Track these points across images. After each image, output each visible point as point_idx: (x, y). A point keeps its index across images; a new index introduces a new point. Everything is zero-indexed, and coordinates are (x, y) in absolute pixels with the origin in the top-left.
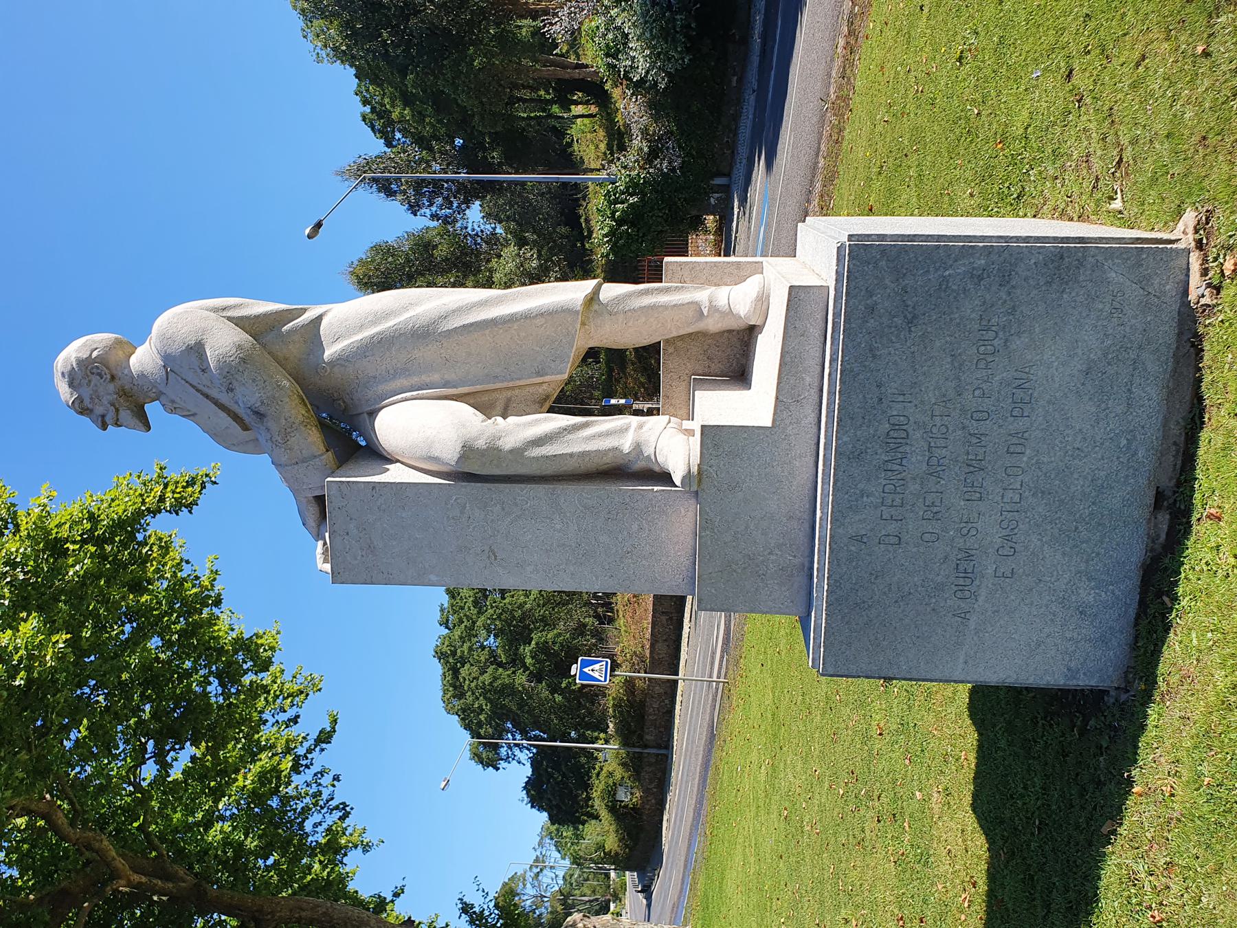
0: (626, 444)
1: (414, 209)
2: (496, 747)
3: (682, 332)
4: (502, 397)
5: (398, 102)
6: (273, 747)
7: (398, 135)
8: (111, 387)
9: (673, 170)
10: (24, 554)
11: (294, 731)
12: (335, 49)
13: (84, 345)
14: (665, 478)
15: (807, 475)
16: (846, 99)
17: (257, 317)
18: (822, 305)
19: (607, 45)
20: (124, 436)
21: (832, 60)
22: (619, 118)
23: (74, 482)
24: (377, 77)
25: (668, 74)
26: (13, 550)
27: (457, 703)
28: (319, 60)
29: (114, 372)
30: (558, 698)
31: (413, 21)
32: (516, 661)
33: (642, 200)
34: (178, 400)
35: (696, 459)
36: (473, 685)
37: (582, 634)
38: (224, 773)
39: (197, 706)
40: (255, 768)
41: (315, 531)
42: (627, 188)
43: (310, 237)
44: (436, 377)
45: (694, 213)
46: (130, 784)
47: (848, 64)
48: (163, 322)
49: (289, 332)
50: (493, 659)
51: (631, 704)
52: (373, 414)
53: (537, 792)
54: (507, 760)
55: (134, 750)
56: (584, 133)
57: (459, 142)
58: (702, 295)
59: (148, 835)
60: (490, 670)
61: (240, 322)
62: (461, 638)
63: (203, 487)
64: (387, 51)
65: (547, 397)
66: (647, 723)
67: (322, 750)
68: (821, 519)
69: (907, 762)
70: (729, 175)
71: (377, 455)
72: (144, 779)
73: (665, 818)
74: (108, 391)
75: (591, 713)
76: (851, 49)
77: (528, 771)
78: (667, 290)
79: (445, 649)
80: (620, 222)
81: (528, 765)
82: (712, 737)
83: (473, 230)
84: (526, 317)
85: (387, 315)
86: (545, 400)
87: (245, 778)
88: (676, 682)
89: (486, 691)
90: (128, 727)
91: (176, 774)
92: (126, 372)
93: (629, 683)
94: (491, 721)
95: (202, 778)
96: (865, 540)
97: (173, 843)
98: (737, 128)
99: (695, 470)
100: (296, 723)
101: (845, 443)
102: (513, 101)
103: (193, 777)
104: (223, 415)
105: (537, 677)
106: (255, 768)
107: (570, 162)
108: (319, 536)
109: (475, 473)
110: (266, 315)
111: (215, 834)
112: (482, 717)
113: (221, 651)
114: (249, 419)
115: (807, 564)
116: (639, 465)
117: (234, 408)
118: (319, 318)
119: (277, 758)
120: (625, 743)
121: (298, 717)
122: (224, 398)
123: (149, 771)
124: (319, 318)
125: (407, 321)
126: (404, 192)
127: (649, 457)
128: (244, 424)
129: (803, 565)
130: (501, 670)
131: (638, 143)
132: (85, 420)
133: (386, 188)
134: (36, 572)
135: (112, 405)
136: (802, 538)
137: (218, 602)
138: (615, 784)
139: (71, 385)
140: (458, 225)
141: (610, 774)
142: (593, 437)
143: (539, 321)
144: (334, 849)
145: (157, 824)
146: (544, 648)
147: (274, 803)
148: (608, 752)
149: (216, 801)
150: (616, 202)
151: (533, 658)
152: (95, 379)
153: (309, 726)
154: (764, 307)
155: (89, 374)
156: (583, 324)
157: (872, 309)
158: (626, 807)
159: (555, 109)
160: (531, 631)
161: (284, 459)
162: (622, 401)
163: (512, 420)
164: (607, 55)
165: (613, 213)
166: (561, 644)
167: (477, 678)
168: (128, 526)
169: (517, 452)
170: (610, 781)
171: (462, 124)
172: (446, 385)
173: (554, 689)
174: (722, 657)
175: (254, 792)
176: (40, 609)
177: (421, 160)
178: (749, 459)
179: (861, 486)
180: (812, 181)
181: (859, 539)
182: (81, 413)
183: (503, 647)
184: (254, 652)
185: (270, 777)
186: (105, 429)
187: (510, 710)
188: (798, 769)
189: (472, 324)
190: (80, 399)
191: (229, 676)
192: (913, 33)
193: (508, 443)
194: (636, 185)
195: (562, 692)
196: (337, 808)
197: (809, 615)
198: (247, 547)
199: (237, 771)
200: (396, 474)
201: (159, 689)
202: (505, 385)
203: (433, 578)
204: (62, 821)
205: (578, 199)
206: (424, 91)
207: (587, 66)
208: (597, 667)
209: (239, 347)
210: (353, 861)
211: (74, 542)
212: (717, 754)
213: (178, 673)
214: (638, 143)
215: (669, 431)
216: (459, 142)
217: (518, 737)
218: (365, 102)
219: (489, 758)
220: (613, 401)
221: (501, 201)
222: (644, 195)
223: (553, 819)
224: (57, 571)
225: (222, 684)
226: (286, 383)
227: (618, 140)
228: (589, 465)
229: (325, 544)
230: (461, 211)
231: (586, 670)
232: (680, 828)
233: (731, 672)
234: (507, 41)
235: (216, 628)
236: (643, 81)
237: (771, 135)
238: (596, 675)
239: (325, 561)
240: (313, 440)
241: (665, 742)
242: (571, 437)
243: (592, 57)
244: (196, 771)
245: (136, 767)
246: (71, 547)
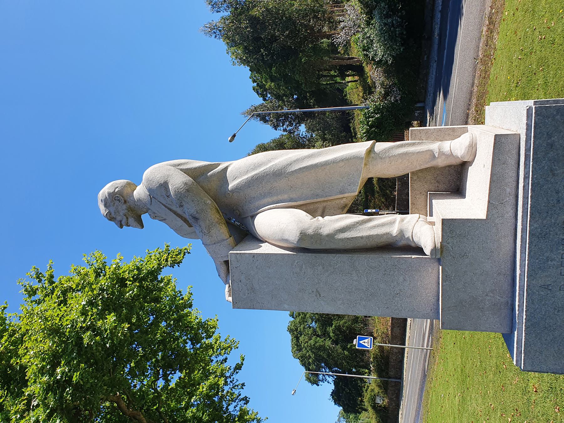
0: (394, 231)
1: (276, 127)
2: (317, 375)
3: (423, 167)
4: (321, 206)
5: (269, 80)
6: (215, 372)
7: (269, 95)
8: (124, 207)
9: (397, 101)
10: (107, 286)
11: (225, 365)
12: (241, 59)
13: (112, 185)
14: (419, 250)
15: (510, 246)
16: (488, 56)
17: (195, 168)
18: (516, 145)
19: (364, 46)
20: (131, 231)
21: (480, 39)
22: (369, 80)
23: (131, 252)
24: (259, 70)
25: (393, 57)
26: (103, 284)
27: (300, 354)
28: (234, 64)
29: (126, 199)
30: (346, 353)
31: (275, 45)
32: (325, 334)
33: (381, 116)
34: (156, 212)
35: (439, 239)
36: (306, 345)
37: (357, 322)
38: (193, 385)
39: (181, 354)
40: (208, 383)
41: (225, 279)
42: (374, 111)
43: (230, 141)
44: (286, 197)
45: (407, 120)
46: (153, 389)
47: (490, 37)
48: (147, 173)
49: (211, 176)
50: (315, 333)
52: (253, 217)
53: (337, 397)
54: (322, 381)
55: (154, 373)
56: (352, 88)
57: (295, 97)
58: (435, 146)
59: (160, 413)
60: (314, 338)
61: (187, 172)
62: (300, 322)
63: (184, 255)
64: (263, 58)
65: (346, 205)
66: (390, 367)
67: (237, 373)
68: (520, 275)
69: (557, 410)
70: (424, 102)
71: (258, 240)
72: (159, 387)
73: (400, 413)
74: (123, 208)
75: (363, 361)
76: (490, 31)
77: (332, 387)
78: (414, 144)
79: (292, 327)
80: (371, 127)
81: (333, 384)
82: (424, 376)
83: (302, 135)
84: (334, 162)
85: (260, 165)
86: (344, 207)
87: (203, 388)
88: (404, 349)
89: (312, 348)
90: (152, 363)
91: (172, 385)
92: (131, 198)
93: (381, 348)
94: (315, 362)
95: (184, 387)
96: (550, 288)
97: (171, 417)
98: (427, 79)
99: (438, 245)
100: (226, 362)
101: (536, 228)
102: (320, 77)
103: (180, 387)
104: (179, 219)
105: (336, 342)
106: (208, 383)
107: (345, 102)
108: (226, 282)
109: (309, 247)
110: (199, 168)
111: (189, 414)
112: (310, 361)
113: (192, 328)
114: (191, 221)
115: (510, 302)
116: (402, 243)
117: (184, 215)
118: (226, 168)
119: (217, 378)
120: (380, 376)
121: (226, 359)
122: (179, 211)
123: (161, 383)
124: (226, 168)
125: (270, 168)
126: (272, 121)
127: (408, 238)
128: (189, 223)
129: (508, 302)
130: (318, 338)
131: (379, 89)
132: (112, 223)
133: (263, 119)
134: (113, 293)
135: (125, 215)
136: (506, 286)
137: (190, 306)
138: (375, 395)
139: (105, 205)
140: (296, 133)
141: (372, 390)
142: (374, 227)
143: (341, 164)
145: (164, 407)
146: (338, 328)
147: (216, 399)
148: (372, 379)
149: (190, 398)
150: (369, 117)
151: (333, 333)
152: (117, 203)
153: (231, 363)
154: (474, 150)
155: (114, 199)
156: (366, 165)
157: (551, 146)
158: (380, 406)
159: (338, 80)
160: (332, 320)
161: (208, 242)
162: (374, 211)
163: (327, 218)
164: (364, 50)
165: (368, 123)
166: (347, 327)
167: (307, 342)
168: (153, 274)
169: (331, 236)
170: (373, 394)
171: (297, 88)
172: (291, 200)
174: (429, 337)
175: (207, 395)
176: (115, 310)
177: (279, 106)
178: (472, 239)
179: (547, 254)
180: (470, 99)
181: (546, 287)
182: (110, 220)
183: (319, 327)
184: (206, 328)
185: (214, 387)
186: (122, 228)
187: (323, 358)
188: (480, 402)
189: (304, 168)
190: (109, 214)
191: (195, 339)
192: (536, 9)
193: (326, 231)
194: (379, 109)
195: (348, 350)
196: (243, 399)
197: (512, 332)
198: (199, 284)
199: (199, 384)
200: (265, 249)
201: (165, 346)
202: (322, 199)
203: (286, 306)
204: (124, 405)
205: (350, 119)
206: (280, 75)
207: (353, 58)
208: (366, 341)
209: (186, 184)
211: (130, 281)
212: (427, 385)
213: (173, 338)
214: (379, 89)
215: (420, 223)
216: (295, 97)
217: (328, 371)
218: (254, 81)
219: (314, 380)
220: (369, 211)
221: (314, 123)
222: (382, 113)
223: (344, 410)
224: (122, 294)
225: (192, 344)
226: (209, 202)
227: (368, 90)
228: (369, 244)
229: (229, 286)
230: (297, 128)
231: (361, 342)
232: (408, 418)
233: (434, 344)
234: (317, 49)
235: (190, 317)
236: (381, 61)
237: (446, 80)
238: (366, 345)
239: (230, 296)
240: (222, 231)
241: (400, 376)
242: (361, 227)
243: (356, 53)
244: (181, 384)
245: (155, 381)
246: (128, 283)
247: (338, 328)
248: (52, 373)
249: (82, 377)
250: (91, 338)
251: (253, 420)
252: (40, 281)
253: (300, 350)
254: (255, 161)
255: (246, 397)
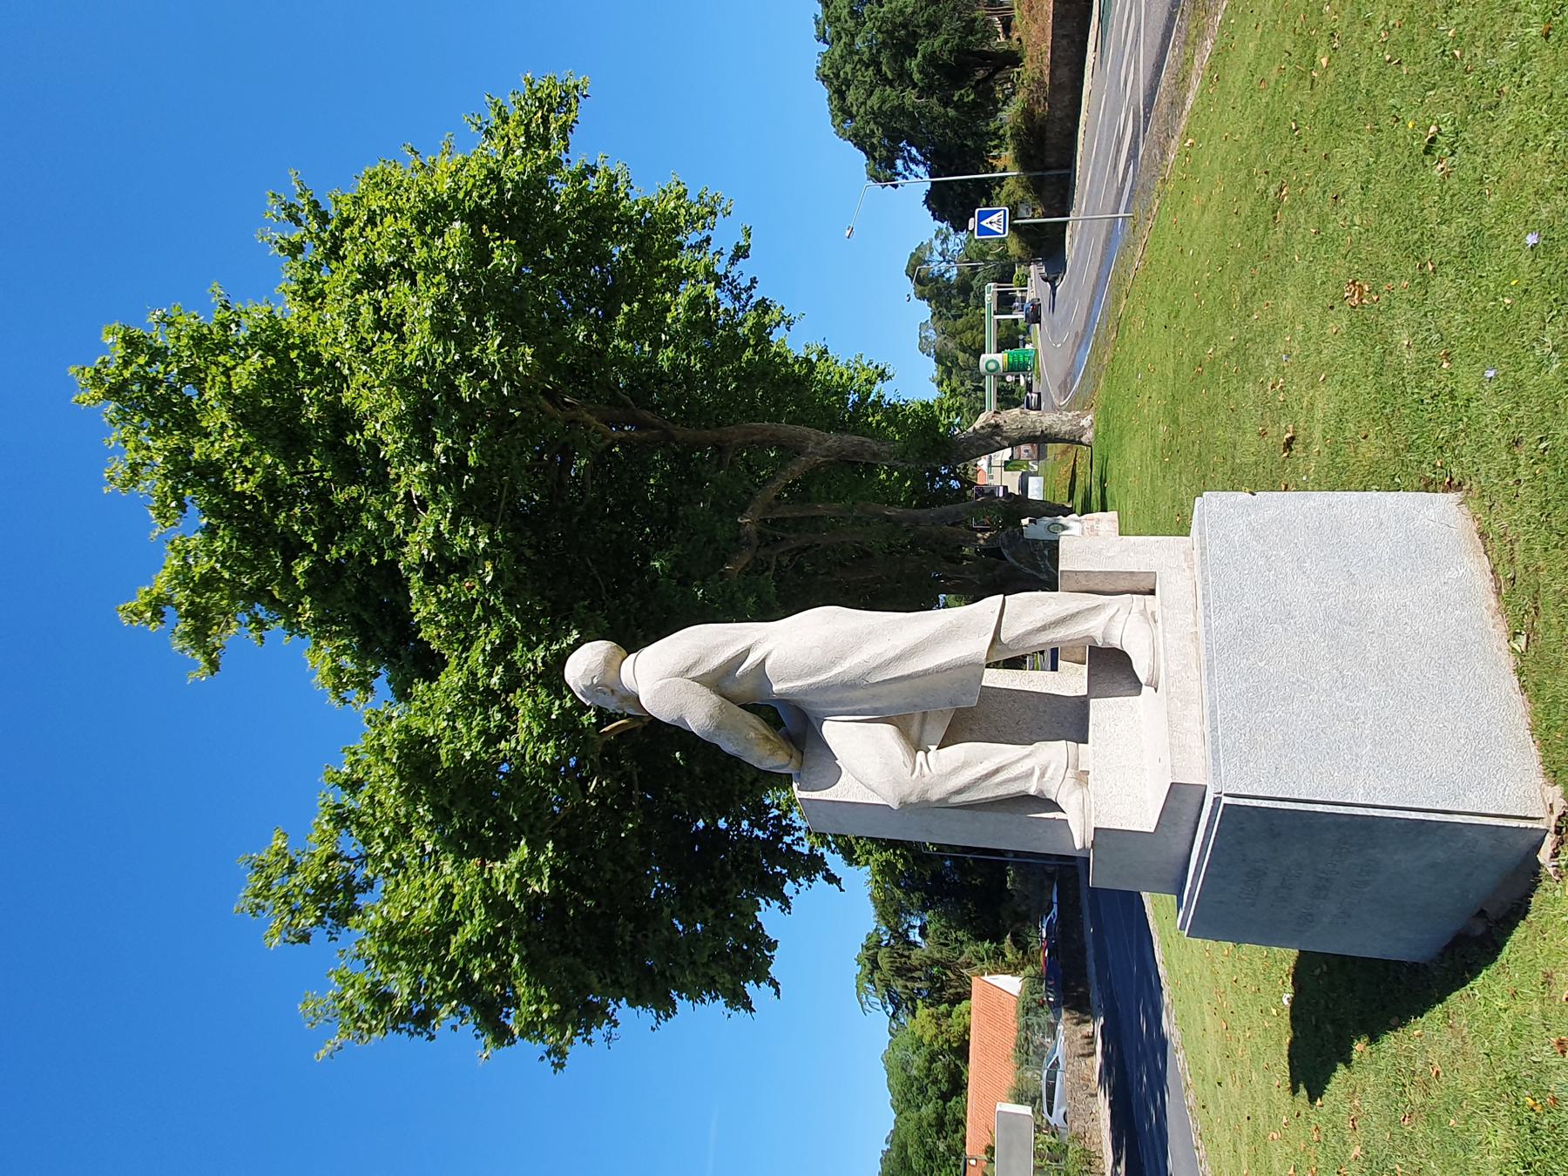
27: (849, 126)
30: (951, 112)
32: (903, 76)
51: (1030, 132)
60: (877, 92)
89: (876, 115)
99: (1089, 845)
112: (875, 141)
144: (761, 331)
146: (931, 59)
167: (864, 103)
173: (945, 103)
187: (902, 132)
208: (994, 218)
210: (777, 336)
219: (884, 169)
231: (983, 223)
238: (994, 227)
241: (1070, 163)
247: (931, 59)
248: (428, 455)
249: (482, 455)
250: (471, 383)
251: (778, 324)
252: (298, 222)
253: (847, 114)
254: (809, 662)
255: (764, 300)
